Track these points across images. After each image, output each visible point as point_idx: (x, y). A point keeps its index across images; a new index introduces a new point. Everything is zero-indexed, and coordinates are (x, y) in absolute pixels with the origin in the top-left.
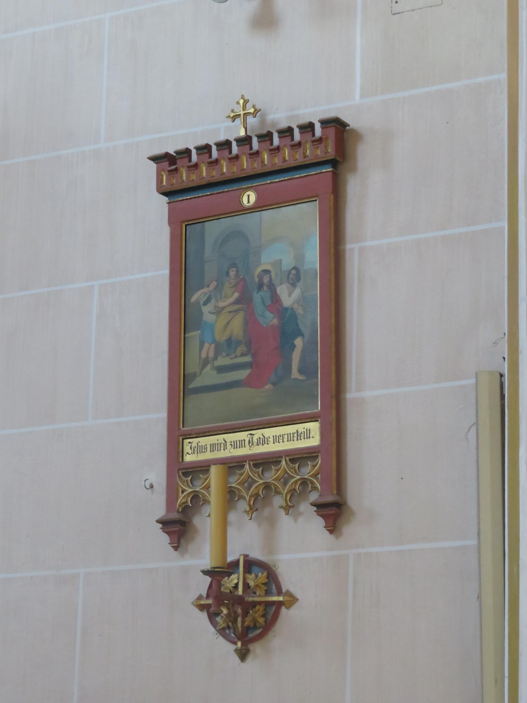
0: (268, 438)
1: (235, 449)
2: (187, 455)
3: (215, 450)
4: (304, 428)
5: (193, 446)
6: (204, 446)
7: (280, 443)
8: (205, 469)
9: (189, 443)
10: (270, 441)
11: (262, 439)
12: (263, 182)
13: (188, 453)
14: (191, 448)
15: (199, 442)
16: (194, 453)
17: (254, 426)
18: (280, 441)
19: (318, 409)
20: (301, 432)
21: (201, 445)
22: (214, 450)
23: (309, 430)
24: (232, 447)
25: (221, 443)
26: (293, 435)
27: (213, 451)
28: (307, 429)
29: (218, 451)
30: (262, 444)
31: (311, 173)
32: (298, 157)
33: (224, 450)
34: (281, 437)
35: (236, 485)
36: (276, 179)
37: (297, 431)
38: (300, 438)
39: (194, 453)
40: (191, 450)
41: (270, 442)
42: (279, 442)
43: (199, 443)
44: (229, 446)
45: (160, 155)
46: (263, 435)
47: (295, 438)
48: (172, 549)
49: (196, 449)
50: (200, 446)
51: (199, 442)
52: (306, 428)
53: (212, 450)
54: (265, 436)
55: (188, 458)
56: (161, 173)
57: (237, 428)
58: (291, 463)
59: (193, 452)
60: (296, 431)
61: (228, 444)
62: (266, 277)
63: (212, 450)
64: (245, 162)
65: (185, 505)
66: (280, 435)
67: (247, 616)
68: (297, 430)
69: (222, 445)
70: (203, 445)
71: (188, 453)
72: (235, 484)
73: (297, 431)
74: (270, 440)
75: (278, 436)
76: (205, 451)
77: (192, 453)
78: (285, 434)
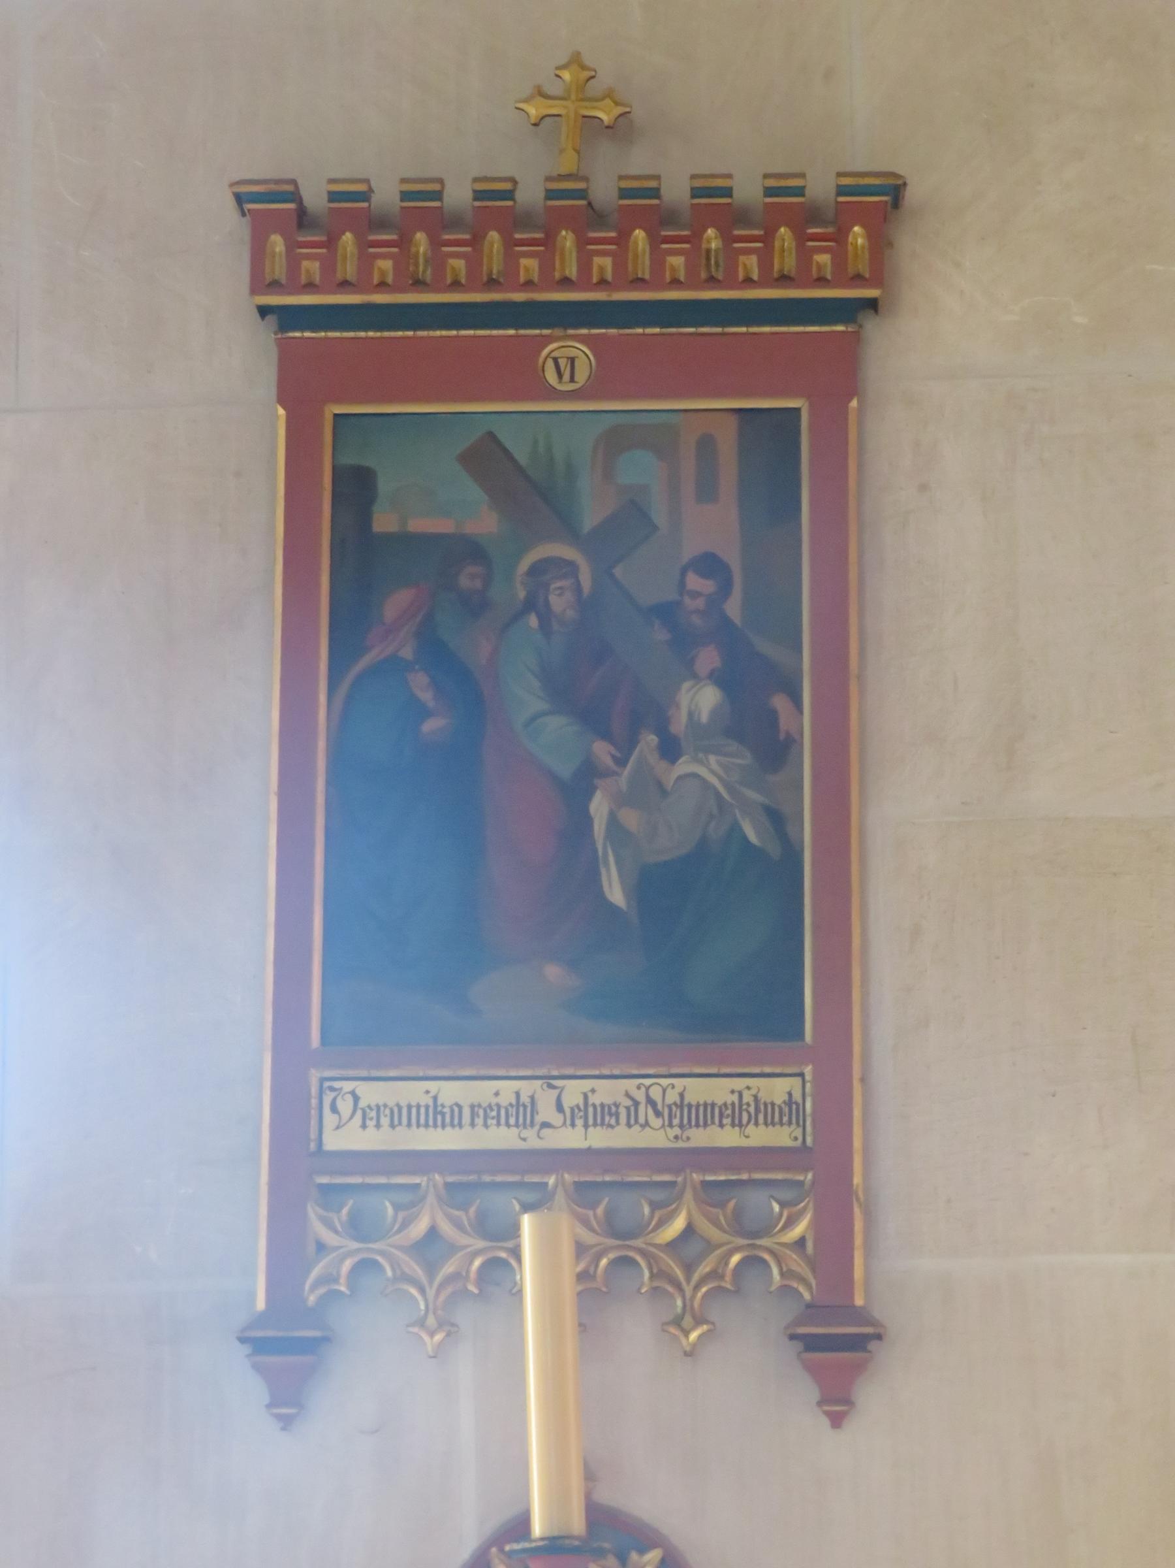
1: (501, 1127)
14: (560, 1108)
15: (593, 1091)
16: (573, 1125)
29: (409, 1125)
34: (727, 1108)
36: (384, 331)
40: (560, 1117)
43: (590, 1094)
48: (825, 1422)
49: (582, 1114)
51: (593, 1091)
52: (432, 1094)
59: (666, 1123)
68: (530, 1094)
75: (720, 1108)
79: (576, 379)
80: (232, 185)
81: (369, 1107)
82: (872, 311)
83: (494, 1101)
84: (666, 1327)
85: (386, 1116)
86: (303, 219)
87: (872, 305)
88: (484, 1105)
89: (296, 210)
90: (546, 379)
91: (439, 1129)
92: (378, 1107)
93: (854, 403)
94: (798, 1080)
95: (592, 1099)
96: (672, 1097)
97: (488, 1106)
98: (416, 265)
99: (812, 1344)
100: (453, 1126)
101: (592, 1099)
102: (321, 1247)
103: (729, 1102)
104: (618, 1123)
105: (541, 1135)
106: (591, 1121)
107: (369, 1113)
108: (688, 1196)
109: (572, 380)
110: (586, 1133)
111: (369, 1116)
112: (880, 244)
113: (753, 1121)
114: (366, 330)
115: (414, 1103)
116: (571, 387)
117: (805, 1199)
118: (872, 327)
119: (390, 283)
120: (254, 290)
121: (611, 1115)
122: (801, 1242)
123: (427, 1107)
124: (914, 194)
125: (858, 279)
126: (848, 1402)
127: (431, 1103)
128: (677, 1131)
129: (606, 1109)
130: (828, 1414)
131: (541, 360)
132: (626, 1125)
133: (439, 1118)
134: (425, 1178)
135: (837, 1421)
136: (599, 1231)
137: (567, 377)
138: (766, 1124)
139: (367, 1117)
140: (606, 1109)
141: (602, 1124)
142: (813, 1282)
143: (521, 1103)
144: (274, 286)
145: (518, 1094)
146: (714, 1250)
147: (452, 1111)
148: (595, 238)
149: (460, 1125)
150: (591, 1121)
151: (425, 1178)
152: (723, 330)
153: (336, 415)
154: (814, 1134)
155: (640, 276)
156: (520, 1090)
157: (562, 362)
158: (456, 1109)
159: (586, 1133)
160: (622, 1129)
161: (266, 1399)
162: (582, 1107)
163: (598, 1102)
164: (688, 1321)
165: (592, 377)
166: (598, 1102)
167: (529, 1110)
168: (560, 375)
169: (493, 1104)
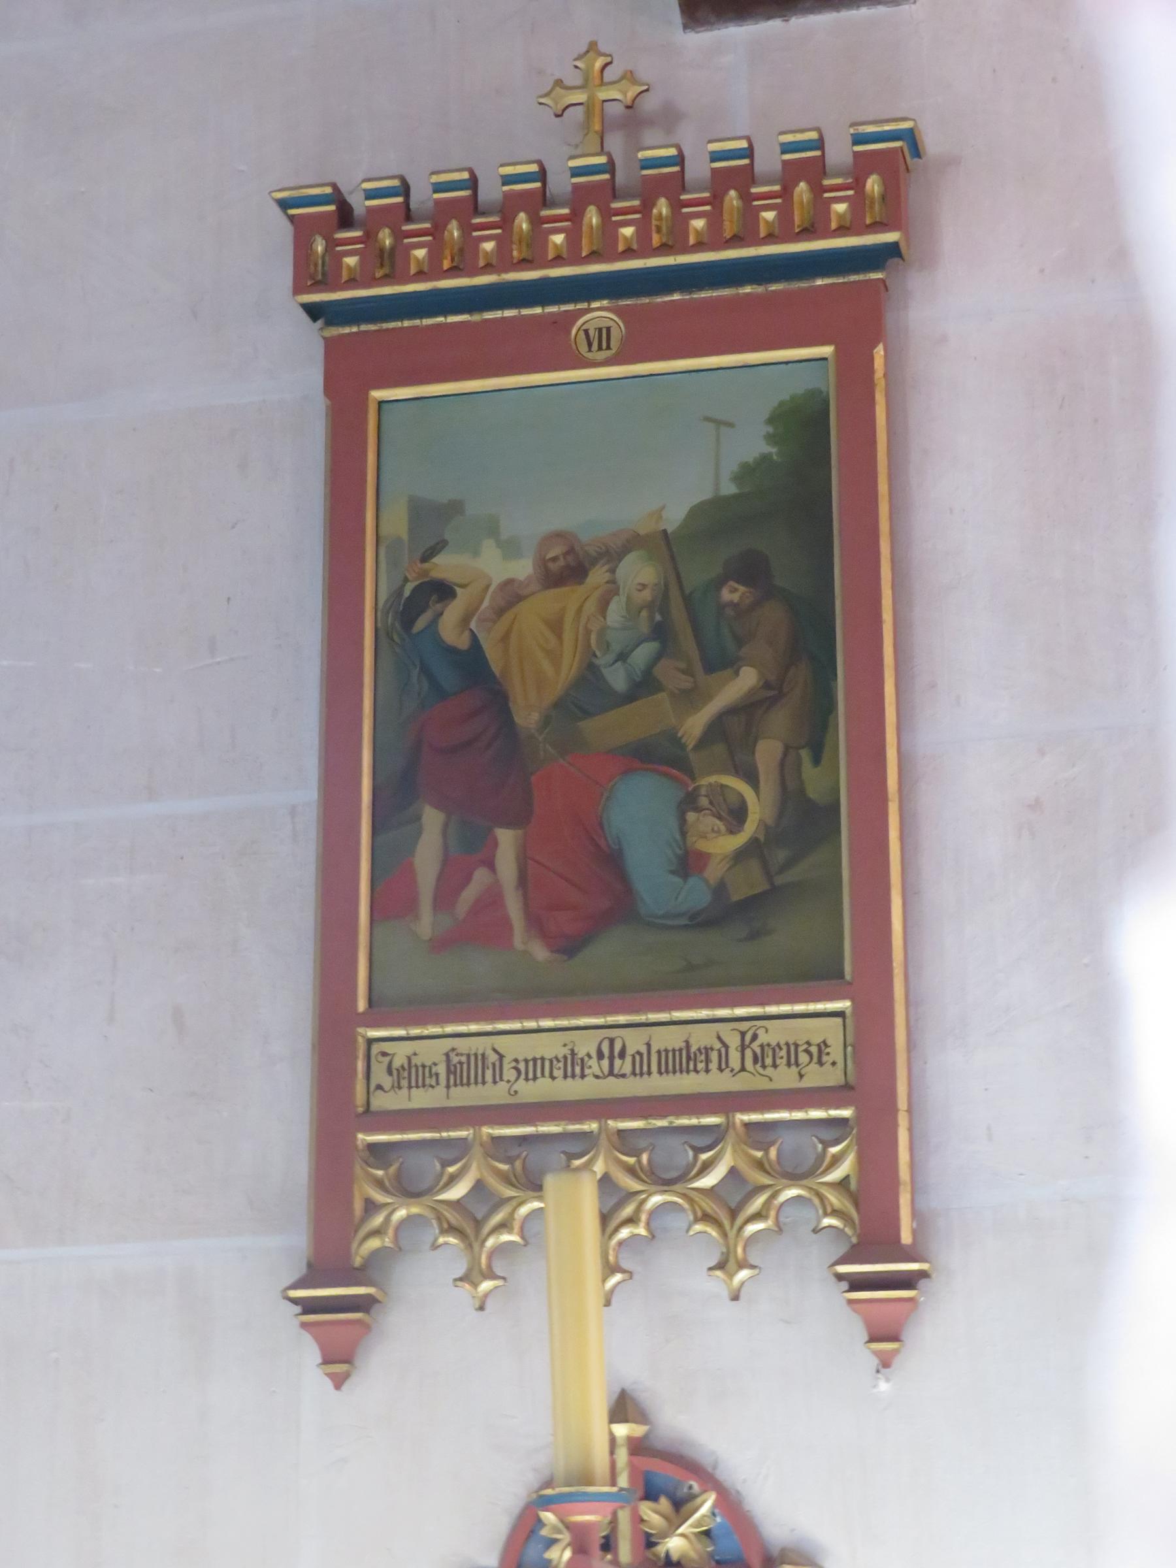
0: (586, 1059)
2: (379, 1092)
4: (565, 1045)
5: (397, 1063)
8: (816, 1114)
9: (384, 1054)
10: (828, 1054)
11: (719, 1051)
13: (379, 1087)
15: (415, 1054)
18: (556, 1073)
20: (699, 1050)
22: (539, 1074)
23: (483, 1055)
24: (810, 1062)
27: (535, 1078)
28: (468, 1056)
33: (495, 1082)
37: (687, 1042)
38: (695, 1065)
39: (400, 1088)
41: (780, 1060)
42: (553, 1078)
43: (413, 1057)
44: (509, 1074)
46: (719, 1038)
48: (328, 1384)
50: (659, 1052)
54: (501, 1051)
60: (569, 1052)
61: (507, 1065)
62: (736, 590)
67: (604, 1537)
69: (714, 1056)
70: (428, 1063)
71: (379, 1087)
73: (687, 1042)
74: (828, 1050)
75: (551, 1061)
76: (433, 1083)
77: (393, 1087)
78: (712, 1049)
79: (612, 346)
81: (778, 1045)
82: (896, 260)
84: (711, 1273)
85: (577, 1064)
86: (345, 217)
87: (893, 250)
88: (774, 1044)
89: (403, 202)
90: (579, 351)
91: (480, 1086)
92: (706, 1048)
93: (879, 351)
94: (839, 1020)
97: (776, 1045)
98: (316, 265)
99: (310, 1307)
101: (415, 1060)
103: (560, 1056)
104: (438, 1084)
106: (413, 1084)
107: (779, 1053)
108: (477, 1151)
109: (608, 348)
110: (409, 1092)
112: (893, 196)
114: (401, 319)
115: (791, 1042)
116: (609, 353)
119: (495, 265)
120: (299, 288)
122: (843, 1184)
124: (932, 143)
125: (878, 226)
126: (348, 1360)
127: (644, 1050)
129: (427, 1070)
130: (331, 1376)
131: (574, 331)
133: (452, 1077)
134: (471, 1131)
135: (339, 1382)
136: (650, 1182)
137: (595, 346)
138: (681, 1072)
140: (427, 1070)
141: (424, 1086)
142: (857, 1221)
144: (320, 284)
145: (743, 1034)
148: (548, 216)
149: (484, 1083)
150: (413, 1084)
151: (471, 1131)
152: (559, 308)
153: (381, 403)
155: (878, 220)
156: (493, 1045)
157: (591, 333)
159: (409, 1092)
160: (441, 1090)
161: (319, 1360)
163: (419, 1064)
164: (732, 1265)
165: (624, 339)
166: (419, 1064)
167: (465, 1066)
168: (590, 345)
169: (702, 1047)
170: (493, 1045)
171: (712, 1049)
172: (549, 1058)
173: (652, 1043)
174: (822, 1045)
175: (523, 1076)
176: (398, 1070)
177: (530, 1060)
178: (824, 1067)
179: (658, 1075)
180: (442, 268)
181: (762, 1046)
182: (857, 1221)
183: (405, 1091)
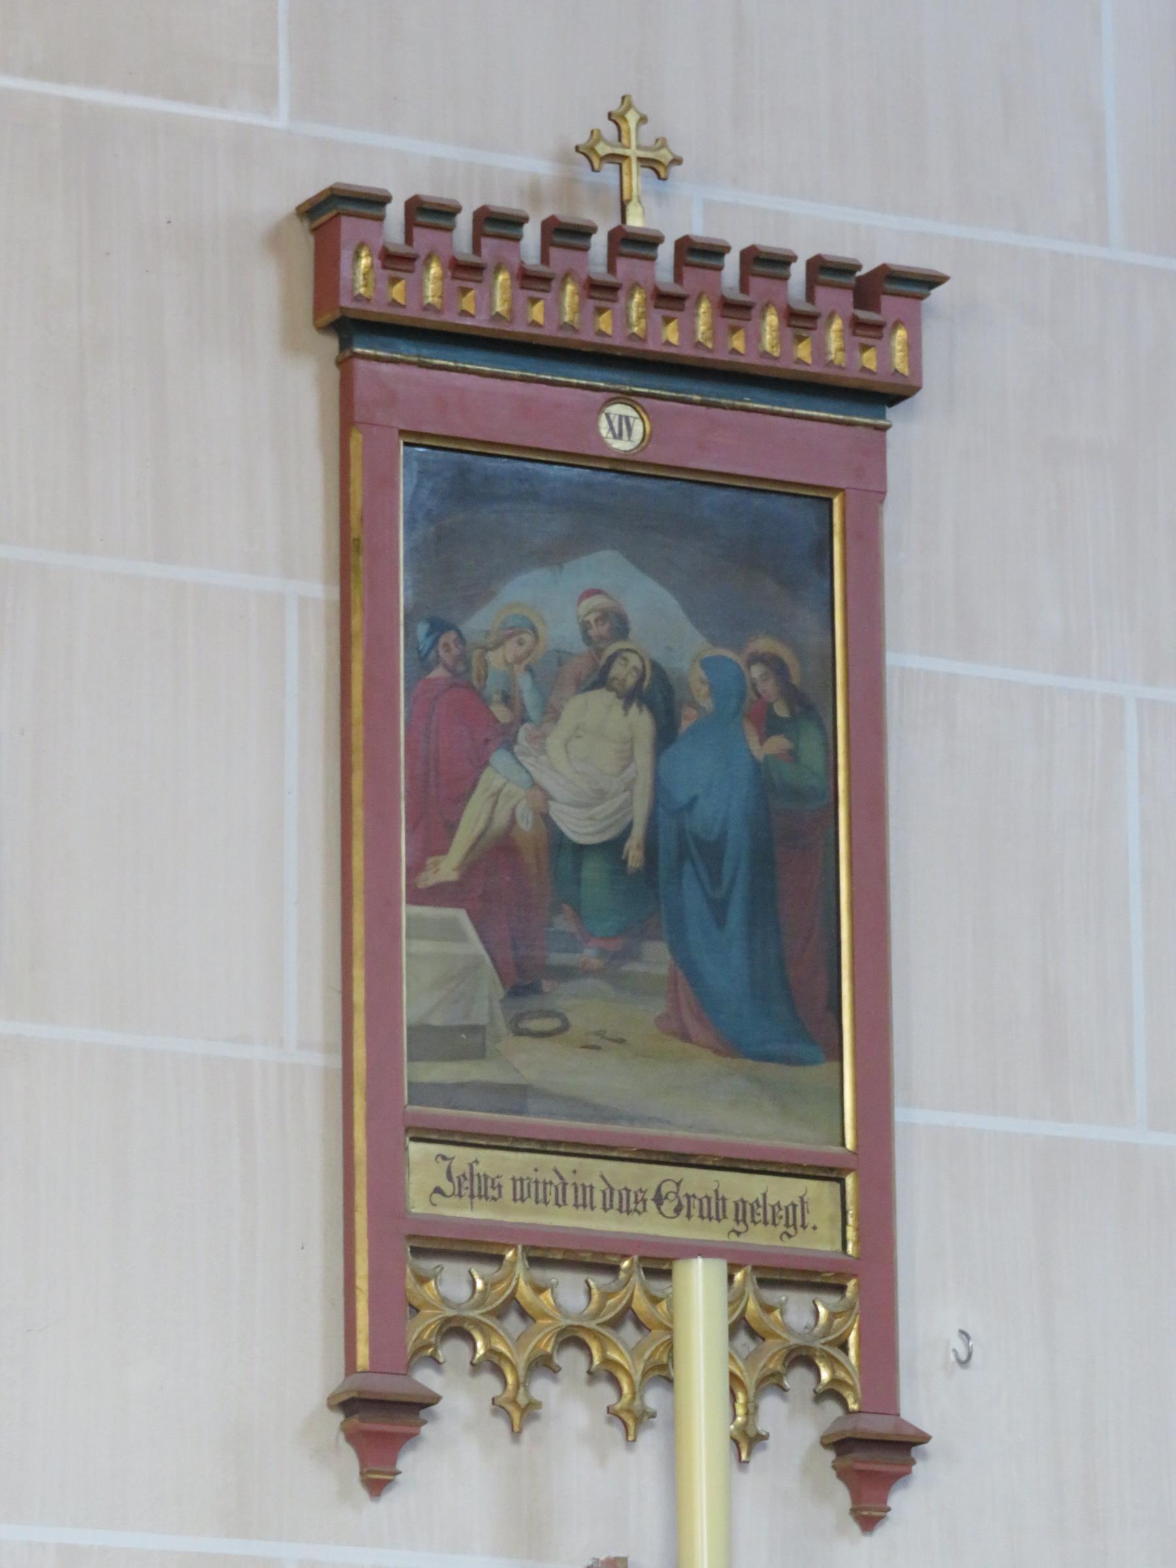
3: (529, 1196)
6: (493, 1180)
7: (778, 1226)
9: (444, 1158)
12: (785, 406)
15: (477, 1162)
17: (613, 1148)
19: (843, 1144)
20: (778, 1204)
21: (481, 1174)
25: (548, 1180)
26: (545, 1188)
27: (522, 1199)
30: (715, 1217)
31: (690, 396)
32: (603, 327)
35: (482, 1314)
39: (460, 1195)
40: (450, 1184)
43: (474, 1165)
45: (839, 260)
46: (557, 1172)
47: (551, 1198)
51: (477, 1162)
53: (518, 1196)
54: (613, 1185)
55: (418, 1204)
56: (774, 305)
57: (505, 1138)
58: (412, 1255)
59: (457, 1192)
63: (518, 1196)
64: (835, 336)
65: (832, 1387)
66: (778, 1204)
68: (763, 1192)
70: (492, 1175)
71: (438, 1190)
72: (823, 1341)
75: (752, 1205)
77: (453, 1193)
80: (749, 320)
83: (533, 1176)
95: (478, 1169)
96: (459, 1168)
100: (584, 1206)
101: (477, 1169)
102: (416, 1310)
105: (434, 1202)
111: (550, 1189)
113: (684, 1212)
115: (517, 1177)
117: (405, 1270)
118: (893, 414)
121: (493, 1187)
123: (794, 1206)
128: (732, 1225)
129: (489, 1182)
132: (734, 1220)
135: (376, 1486)
138: (702, 1217)
139: (755, 1213)
140: (489, 1182)
143: (720, 1197)
146: (833, 1340)
147: (621, 1195)
149: (546, 1203)
150: (476, 1192)
154: (859, 1241)
156: (601, 1172)
158: (741, 1205)
162: (761, 1202)
165: (647, 438)
170: (601, 1172)
171: (551, 1183)
172: (751, 1202)
173: (768, 1194)
174: (755, 1205)
175: (684, 1212)
176: (773, 1207)
177: (588, 1186)
178: (463, 1198)
179: (602, 1212)
180: (406, 282)
181: (688, 1196)
182: (858, 1387)
183: (466, 1199)
